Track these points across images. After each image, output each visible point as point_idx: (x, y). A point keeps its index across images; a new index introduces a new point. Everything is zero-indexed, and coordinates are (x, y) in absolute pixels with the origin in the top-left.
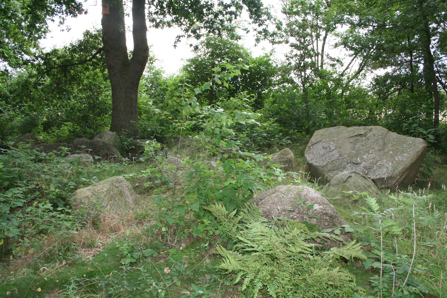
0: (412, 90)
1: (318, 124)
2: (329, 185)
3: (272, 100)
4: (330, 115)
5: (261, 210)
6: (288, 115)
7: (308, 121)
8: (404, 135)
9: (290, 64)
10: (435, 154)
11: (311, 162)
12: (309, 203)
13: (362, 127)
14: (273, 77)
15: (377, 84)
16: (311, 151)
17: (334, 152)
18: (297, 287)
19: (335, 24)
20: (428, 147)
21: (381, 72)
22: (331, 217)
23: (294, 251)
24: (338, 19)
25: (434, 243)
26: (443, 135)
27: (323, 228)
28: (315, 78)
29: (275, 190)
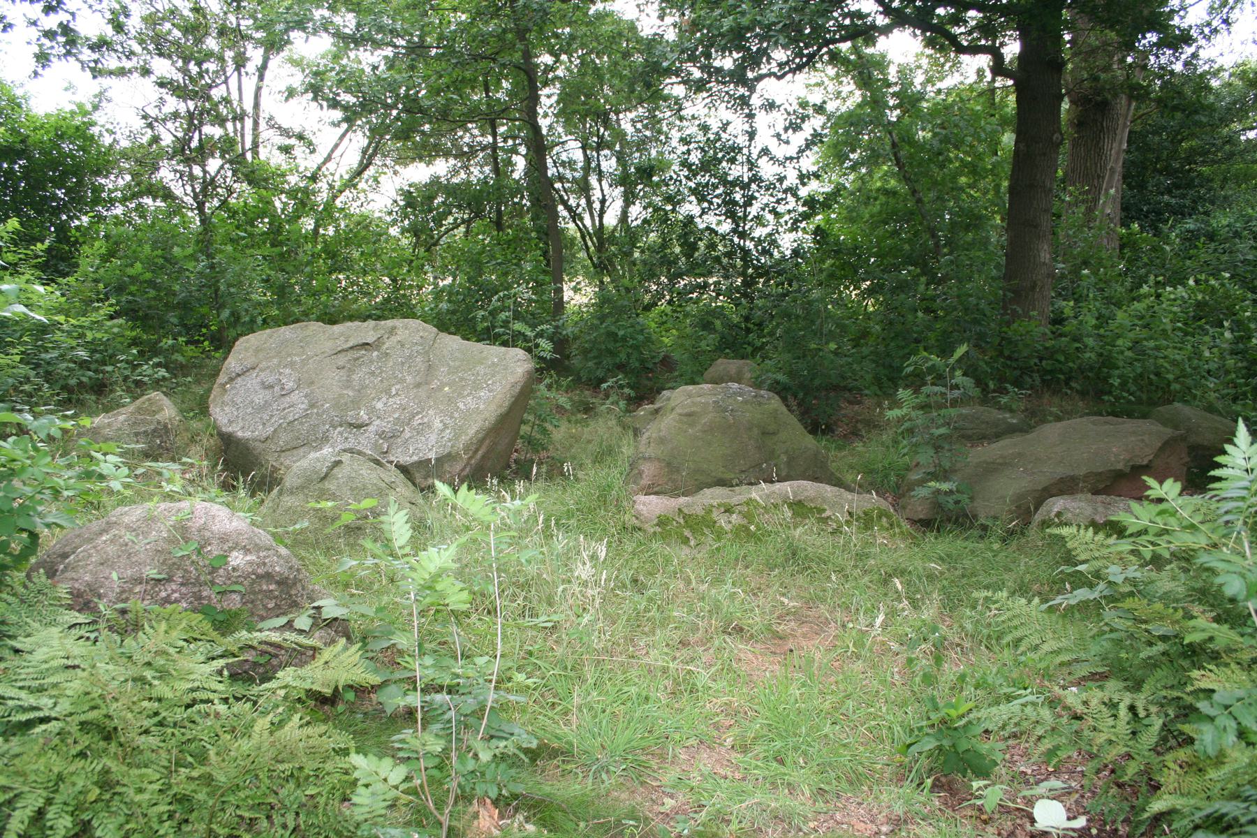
0: (499, 225)
1: (247, 319)
2: (281, 493)
3: (103, 251)
4: (282, 292)
5: (62, 590)
6: (152, 293)
7: (218, 309)
8: (478, 341)
9: (156, 139)
10: (557, 390)
11: (230, 429)
12: (214, 550)
13: (371, 323)
14: (106, 177)
15: (408, 205)
16: (226, 398)
17: (295, 397)
18: (186, 804)
19: (286, 31)
20: (537, 370)
21: (419, 173)
22: (283, 583)
23: (169, 695)
24: (296, 18)
25: (555, 618)
26: (575, 338)
27: (263, 619)
28: (235, 185)
29: (108, 523)
